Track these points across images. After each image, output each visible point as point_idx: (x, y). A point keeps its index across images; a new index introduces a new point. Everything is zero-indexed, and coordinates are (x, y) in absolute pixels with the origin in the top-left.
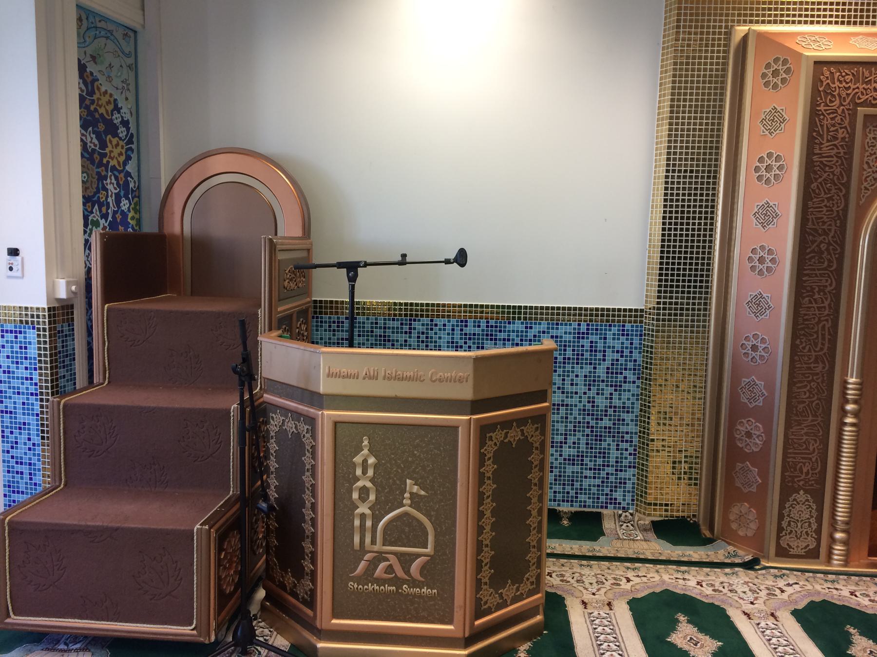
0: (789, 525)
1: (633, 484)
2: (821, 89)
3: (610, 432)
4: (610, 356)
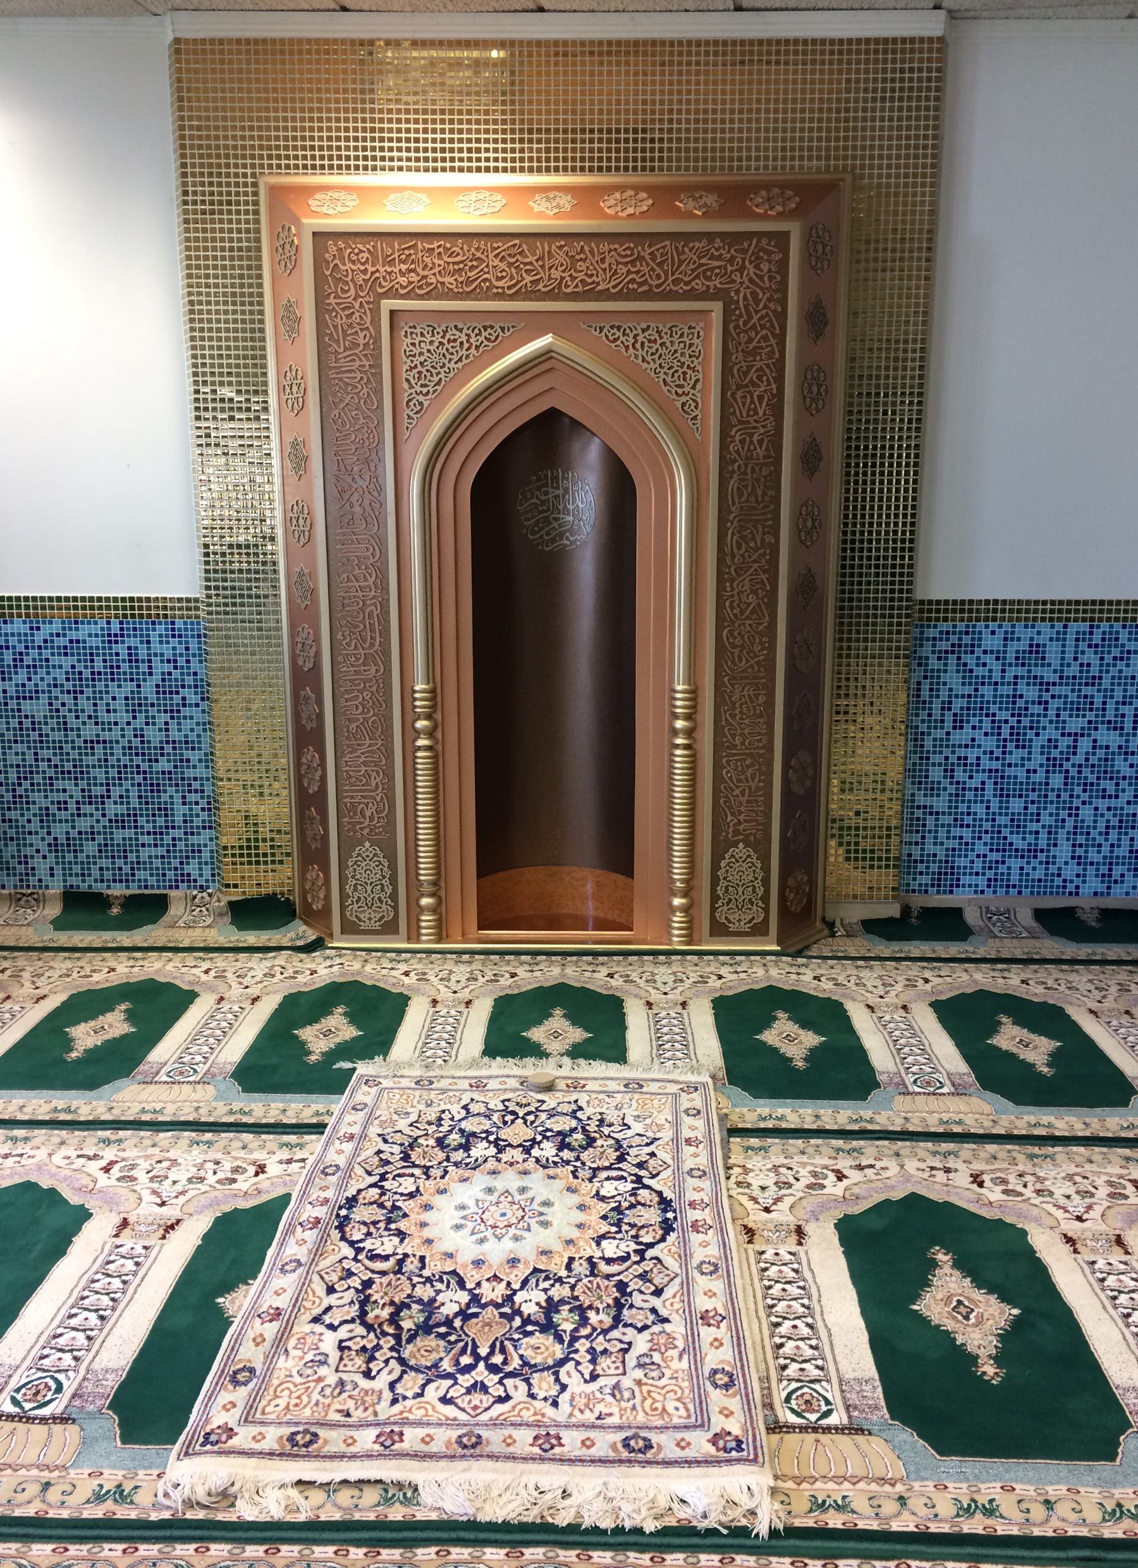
0: (355, 890)
1: (212, 851)
2: (328, 273)
3: (170, 779)
4: (159, 668)
